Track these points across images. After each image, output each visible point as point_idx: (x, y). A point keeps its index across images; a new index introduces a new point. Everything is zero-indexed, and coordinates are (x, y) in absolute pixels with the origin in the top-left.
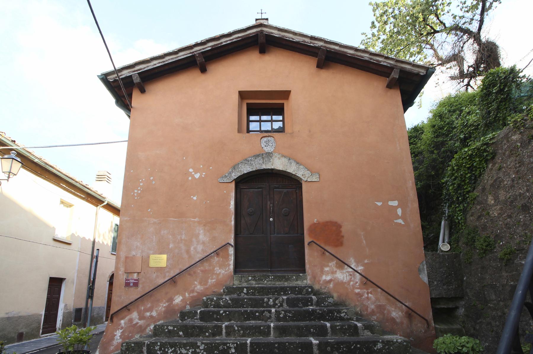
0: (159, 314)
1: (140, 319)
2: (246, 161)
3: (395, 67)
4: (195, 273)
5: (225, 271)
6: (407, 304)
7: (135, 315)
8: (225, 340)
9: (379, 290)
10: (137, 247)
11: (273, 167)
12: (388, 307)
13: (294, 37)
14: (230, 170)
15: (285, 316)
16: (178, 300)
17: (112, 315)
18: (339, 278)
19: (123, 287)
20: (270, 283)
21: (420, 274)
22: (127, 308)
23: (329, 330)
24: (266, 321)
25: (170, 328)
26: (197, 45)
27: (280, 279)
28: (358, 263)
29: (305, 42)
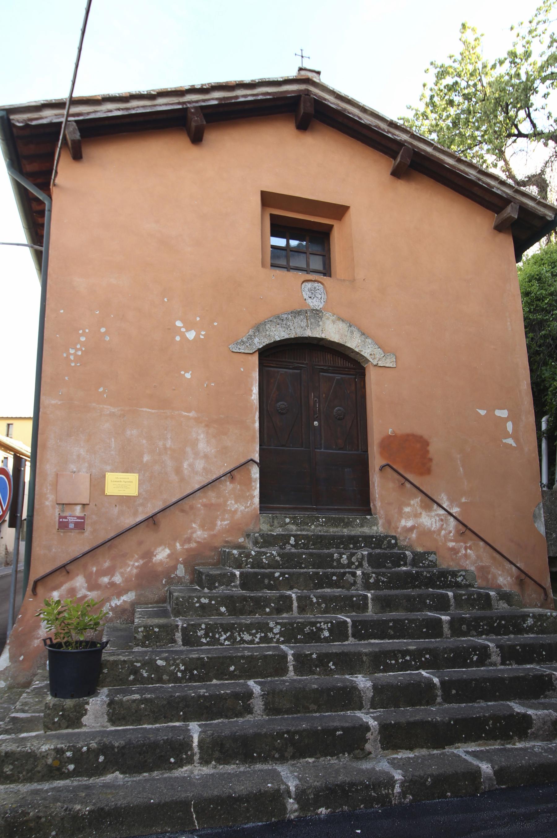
0: (126, 580)
1: (90, 589)
2: (278, 319)
3: (512, 200)
4: (192, 508)
5: (246, 507)
6: (518, 565)
7: (79, 582)
8: (296, 618)
9: (482, 543)
10: (79, 456)
11: (323, 336)
12: (493, 570)
13: (361, 115)
14: (251, 333)
15: (377, 581)
16: (162, 555)
17: (36, 583)
18: (426, 524)
19: (55, 531)
20: (319, 528)
21: (535, 522)
22: (65, 569)
23: (452, 601)
24: (348, 589)
25: (203, 600)
26: (193, 90)
27: (336, 522)
28: (452, 501)
29: (379, 128)
